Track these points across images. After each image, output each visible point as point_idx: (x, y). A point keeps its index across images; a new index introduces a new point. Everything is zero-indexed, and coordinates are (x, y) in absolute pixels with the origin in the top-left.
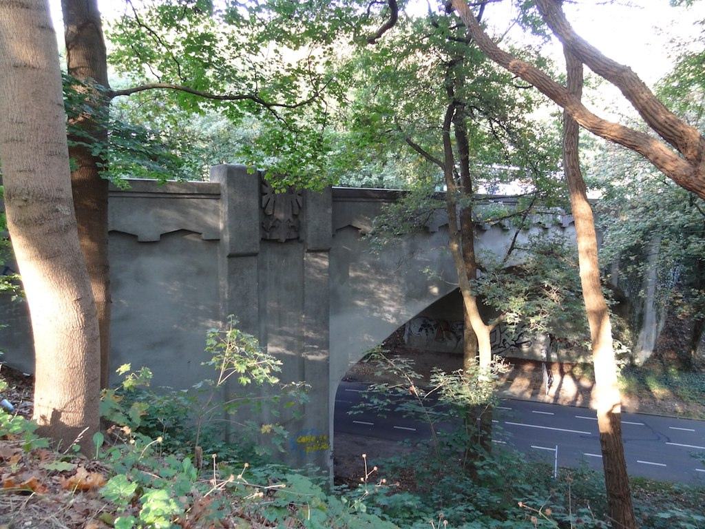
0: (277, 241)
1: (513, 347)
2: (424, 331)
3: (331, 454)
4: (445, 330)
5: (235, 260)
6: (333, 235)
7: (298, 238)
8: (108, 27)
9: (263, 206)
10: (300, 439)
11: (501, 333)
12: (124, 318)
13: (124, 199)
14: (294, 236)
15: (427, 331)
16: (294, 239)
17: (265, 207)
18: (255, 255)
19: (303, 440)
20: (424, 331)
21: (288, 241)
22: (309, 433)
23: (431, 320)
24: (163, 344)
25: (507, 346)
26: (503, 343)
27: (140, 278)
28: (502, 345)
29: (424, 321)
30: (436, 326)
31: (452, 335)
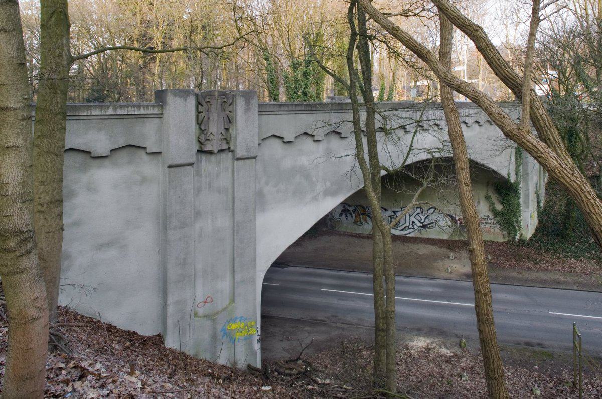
0: (210, 152)
1: (420, 228)
2: (344, 216)
3: (258, 337)
4: (363, 214)
5: (173, 169)
6: (259, 144)
7: (229, 148)
8: (235, 222)
9: (199, 122)
10: (231, 326)
11: (410, 216)
12: (77, 224)
13: (82, 121)
14: (225, 146)
15: (346, 216)
16: (225, 149)
17: (201, 124)
18: (191, 164)
19: (233, 327)
20: (344, 216)
21: (221, 151)
22: (238, 320)
23: (350, 206)
24: (109, 245)
25: (416, 227)
26: (412, 225)
27: (91, 188)
28: (411, 226)
29: (344, 207)
30: (354, 211)
31: (368, 219)
